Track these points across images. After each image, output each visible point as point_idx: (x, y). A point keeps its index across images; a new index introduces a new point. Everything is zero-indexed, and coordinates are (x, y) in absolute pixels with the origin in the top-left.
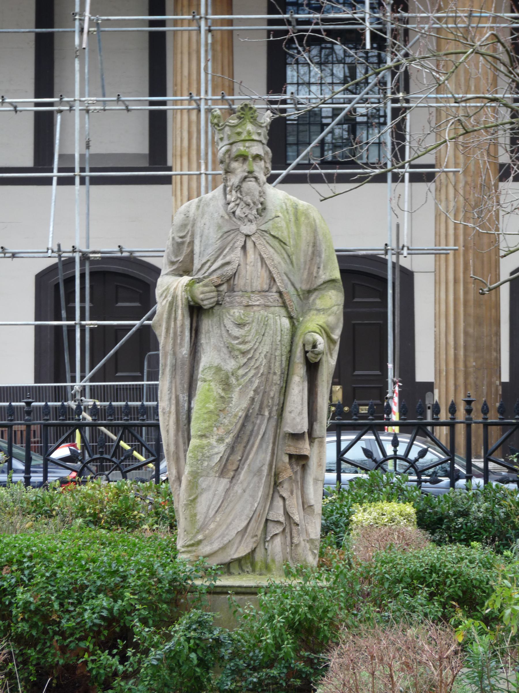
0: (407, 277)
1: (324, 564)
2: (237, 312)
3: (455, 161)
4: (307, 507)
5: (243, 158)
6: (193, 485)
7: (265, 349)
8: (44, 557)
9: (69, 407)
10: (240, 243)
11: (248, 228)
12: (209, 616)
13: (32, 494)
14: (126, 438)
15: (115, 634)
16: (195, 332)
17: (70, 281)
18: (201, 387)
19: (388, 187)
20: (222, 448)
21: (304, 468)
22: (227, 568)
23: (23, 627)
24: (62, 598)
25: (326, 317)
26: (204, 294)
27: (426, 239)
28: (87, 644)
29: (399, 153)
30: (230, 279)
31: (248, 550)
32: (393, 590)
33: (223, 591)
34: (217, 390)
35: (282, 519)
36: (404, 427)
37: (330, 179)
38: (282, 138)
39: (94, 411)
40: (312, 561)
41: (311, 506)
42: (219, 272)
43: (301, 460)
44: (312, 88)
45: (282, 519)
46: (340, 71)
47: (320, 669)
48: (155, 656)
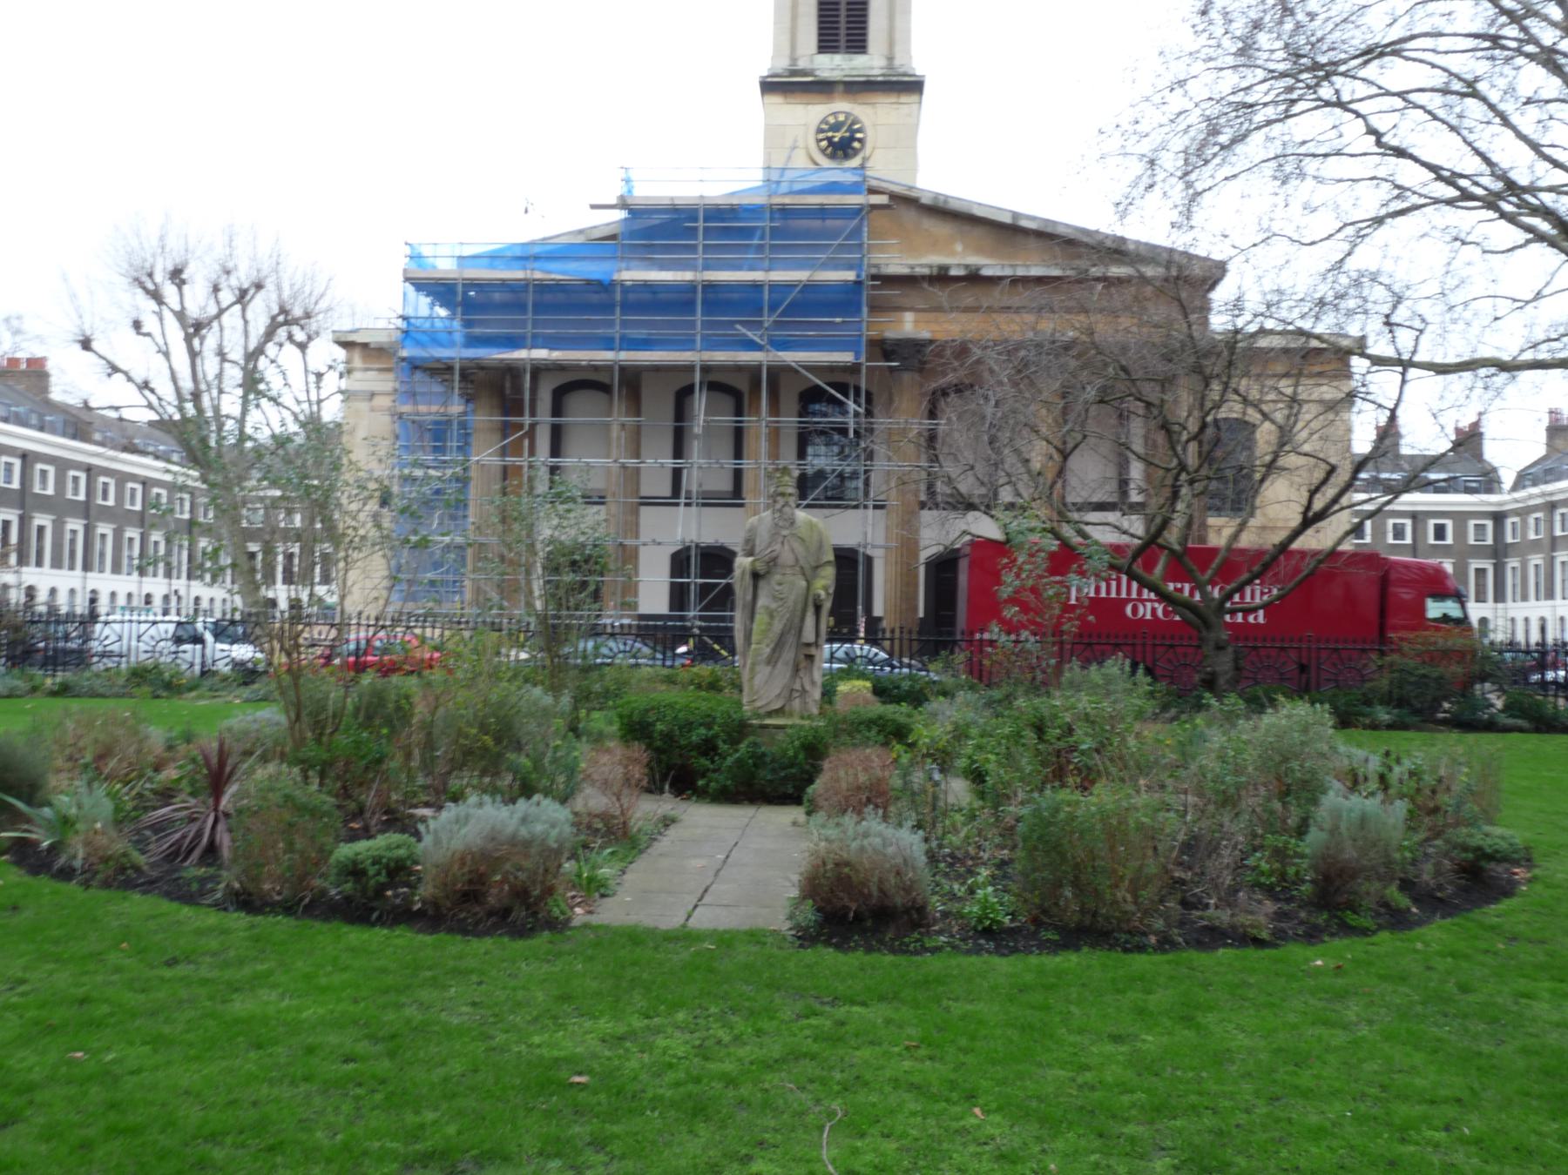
0: (869, 561)
1: (822, 714)
2: (777, 577)
4: (813, 683)
5: (783, 494)
6: (752, 670)
7: (792, 597)
8: (671, 706)
9: (36, 843)
11: (785, 532)
12: (759, 740)
13: (665, 672)
14: (716, 642)
15: (708, 748)
16: (755, 588)
17: (688, 558)
18: (758, 617)
19: (860, 511)
20: (768, 650)
22: (770, 714)
23: (658, 743)
24: (680, 728)
25: (825, 581)
26: (760, 567)
27: (881, 541)
28: (694, 753)
29: (866, 494)
30: (774, 559)
32: (857, 728)
33: (766, 726)
34: (766, 618)
36: (867, 641)
37: (830, 507)
38: (805, 485)
39: (700, 628)
40: (815, 711)
43: (810, 658)
44: (820, 458)
46: (836, 449)
47: (817, 770)
48: (729, 761)
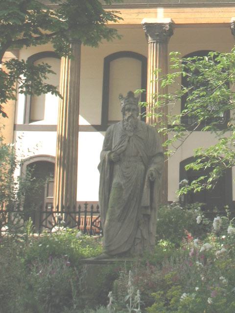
3: (118, 17)
10: (127, 139)
20: (119, 211)
21: (149, 219)
31: (128, 249)
35: (140, 237)
41: (151, 233)
42: (119, 150)
43: (148, 217)
45: (140, 237)
